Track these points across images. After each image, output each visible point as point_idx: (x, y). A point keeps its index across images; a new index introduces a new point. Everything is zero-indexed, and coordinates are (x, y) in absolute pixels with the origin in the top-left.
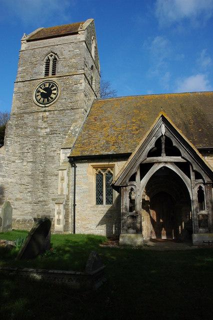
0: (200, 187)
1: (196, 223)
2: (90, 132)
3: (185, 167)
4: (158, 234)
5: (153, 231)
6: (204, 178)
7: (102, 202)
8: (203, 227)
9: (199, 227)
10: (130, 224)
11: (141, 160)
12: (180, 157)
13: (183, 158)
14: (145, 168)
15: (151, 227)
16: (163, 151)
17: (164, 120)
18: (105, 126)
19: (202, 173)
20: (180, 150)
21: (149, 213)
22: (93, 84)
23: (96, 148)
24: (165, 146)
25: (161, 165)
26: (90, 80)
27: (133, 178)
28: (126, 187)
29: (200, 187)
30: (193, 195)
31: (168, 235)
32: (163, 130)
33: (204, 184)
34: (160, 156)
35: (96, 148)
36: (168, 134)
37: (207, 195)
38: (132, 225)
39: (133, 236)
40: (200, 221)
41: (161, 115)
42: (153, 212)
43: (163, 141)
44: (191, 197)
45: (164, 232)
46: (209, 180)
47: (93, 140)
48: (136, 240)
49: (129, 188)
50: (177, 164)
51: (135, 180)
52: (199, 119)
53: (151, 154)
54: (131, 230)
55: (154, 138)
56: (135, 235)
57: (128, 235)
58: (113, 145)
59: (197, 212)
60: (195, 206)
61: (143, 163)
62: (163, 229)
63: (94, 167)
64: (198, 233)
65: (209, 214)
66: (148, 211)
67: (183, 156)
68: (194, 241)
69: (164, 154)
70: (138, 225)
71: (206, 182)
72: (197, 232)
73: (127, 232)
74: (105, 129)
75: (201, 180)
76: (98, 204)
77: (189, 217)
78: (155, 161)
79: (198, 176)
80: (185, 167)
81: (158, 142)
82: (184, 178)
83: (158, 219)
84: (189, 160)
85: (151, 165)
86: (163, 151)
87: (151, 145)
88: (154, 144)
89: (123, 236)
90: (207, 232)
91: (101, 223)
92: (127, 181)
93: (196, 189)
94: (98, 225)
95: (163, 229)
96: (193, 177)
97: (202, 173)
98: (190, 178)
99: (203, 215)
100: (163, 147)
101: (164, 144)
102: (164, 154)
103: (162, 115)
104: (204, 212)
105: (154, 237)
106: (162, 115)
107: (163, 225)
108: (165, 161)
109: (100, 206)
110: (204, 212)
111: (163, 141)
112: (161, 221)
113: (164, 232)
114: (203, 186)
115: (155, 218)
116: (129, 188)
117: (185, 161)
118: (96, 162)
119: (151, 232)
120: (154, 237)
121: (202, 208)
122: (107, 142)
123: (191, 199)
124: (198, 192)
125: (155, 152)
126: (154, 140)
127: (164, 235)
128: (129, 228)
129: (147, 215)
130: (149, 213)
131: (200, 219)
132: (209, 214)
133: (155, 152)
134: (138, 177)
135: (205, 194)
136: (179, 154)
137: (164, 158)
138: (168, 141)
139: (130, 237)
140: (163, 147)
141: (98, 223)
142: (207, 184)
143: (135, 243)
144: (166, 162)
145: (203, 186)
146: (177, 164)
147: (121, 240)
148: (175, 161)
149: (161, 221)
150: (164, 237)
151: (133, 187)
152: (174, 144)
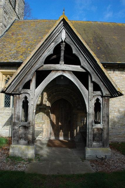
0: (98, 100)
1: (90, 137)
2: (5, 44)
3: (83, 77)
4: (57, 135)
5: (52, 132)
6: (102, 90)
7: (10, 105)
8: (98, 141)
9: (93, 141)
10: (21, 134)
11: (37, 66)
12: (79, 66)
13: (82, 67)
14: (41, 75)
15: (50, 129)
16: (62, 58)
17: (66, 25)
18: (19, 40)
19: (101, 85)
20: (80, 58)
21: (50, 118)
22: (17, 7)
23: (6, 57)
24: (65, 53)
25: (59, 74)
26: (13, 5)
27: (27, 86)
28: (19, 94)
29: (98, 100)
30: (90, 108)
31: (65, 136)
32: (64, 35)
33: (102, 96)
34: (58, 63)
35: (6, 57)
36: (69, 41)
37: (104, 107)
38: (23, 136)
39: (24, 147)
40: (94, 135)
41: (62, 18)
42: (53, 116)
43: (63, 48)
44: (87, 109)
45: (61, 133)
46: (108, 93)
47: (6, 50)
48: (27, 152)
49: (22, 96)
50: (76, 73)
51: (29, 88)
52: (98, 40)
53: (48, 60)
54: (22, 141)
55: (53, 43)
56: (26, 146)
57: (19, 146)
58: (22, 55)
59: (92, 126)
60: (90, 119)
61: (39, 70)
62: (61, 131)
63: (4, 74)
64: (91, 147)
65: (104, 128)
66: (48, 115)
67: (82, 65)
68: (87, 155)
69: (62, 62)
70: (30, 136)
71: (104, 94)
72: (91, 146)
73: (18, 143)
74: (18, 42)
75: (99, 93)
76: (5, 107)
77: (84, 122)
78: (52, 69)
79: (96, 88)
80: (83, 77)
81: (57, 49)
82: (81, 88)
83: (57, 123)
84: (89, 71)
85: (48, 72)
86: (62, 58)
87: (49, 51)
88: (52, 50)
89: (13, 147)
90: (100, 147)
91: (6, 124)
92: (21, 89)
93: (93, 101)
94: (5, 125)
95: (61, 131)
96: (91, 88)
97: (101, 85)
98: (87, 88)
99: (98, 129)
100: (62, 54)
101: (63, 51)
102: (62, 62)
103: (64, 20)
104: (99, 126)
105: (53, 138)
106: (64, 20)
107: (61, 128)
108: (64, 69)
109: (7, 108)
110: (99, 126)
111: (63, 48)
112: (60, 124)
113: (61, 133)
114: (101, 99)
115: (55, 121)
116: (22, 96)
117: (84, 71)
118: (6, 69)
119: (51, 134)
120: (53, 138)
121: (97, 123)
122: (17, 52)
123: (88, 111)
124: (95, 104)
125: (52, 59)
126: (53, 46)
127: (61, 135)
128: (20, 138)
129: (47, 119)
130: (50, 118)
131: (95, 132)
132: (104, 128)
133: (52, 59)
134: (33, 84)
135: (102, 107)
136: (78, 63)
137: (62, 66)
138: (68, 48)
139: (20, 149)
140: (62, 54)
141: (4, 123)
142: (105, 96)
143: (26, 155)
144: (64, 71)
145: (101, 99)
146: (76, 73)
147: (11, 151)
148: (74, 70)
149: (60, 124)
150: (61, 138)
151: (27, 95)
152: (74, 52)
